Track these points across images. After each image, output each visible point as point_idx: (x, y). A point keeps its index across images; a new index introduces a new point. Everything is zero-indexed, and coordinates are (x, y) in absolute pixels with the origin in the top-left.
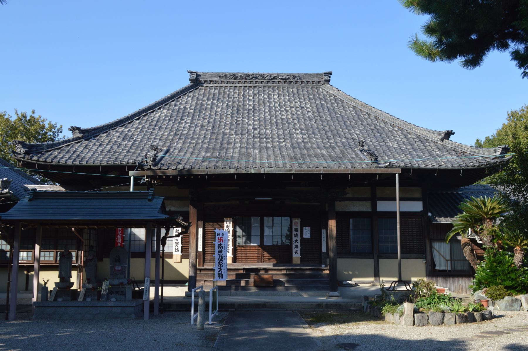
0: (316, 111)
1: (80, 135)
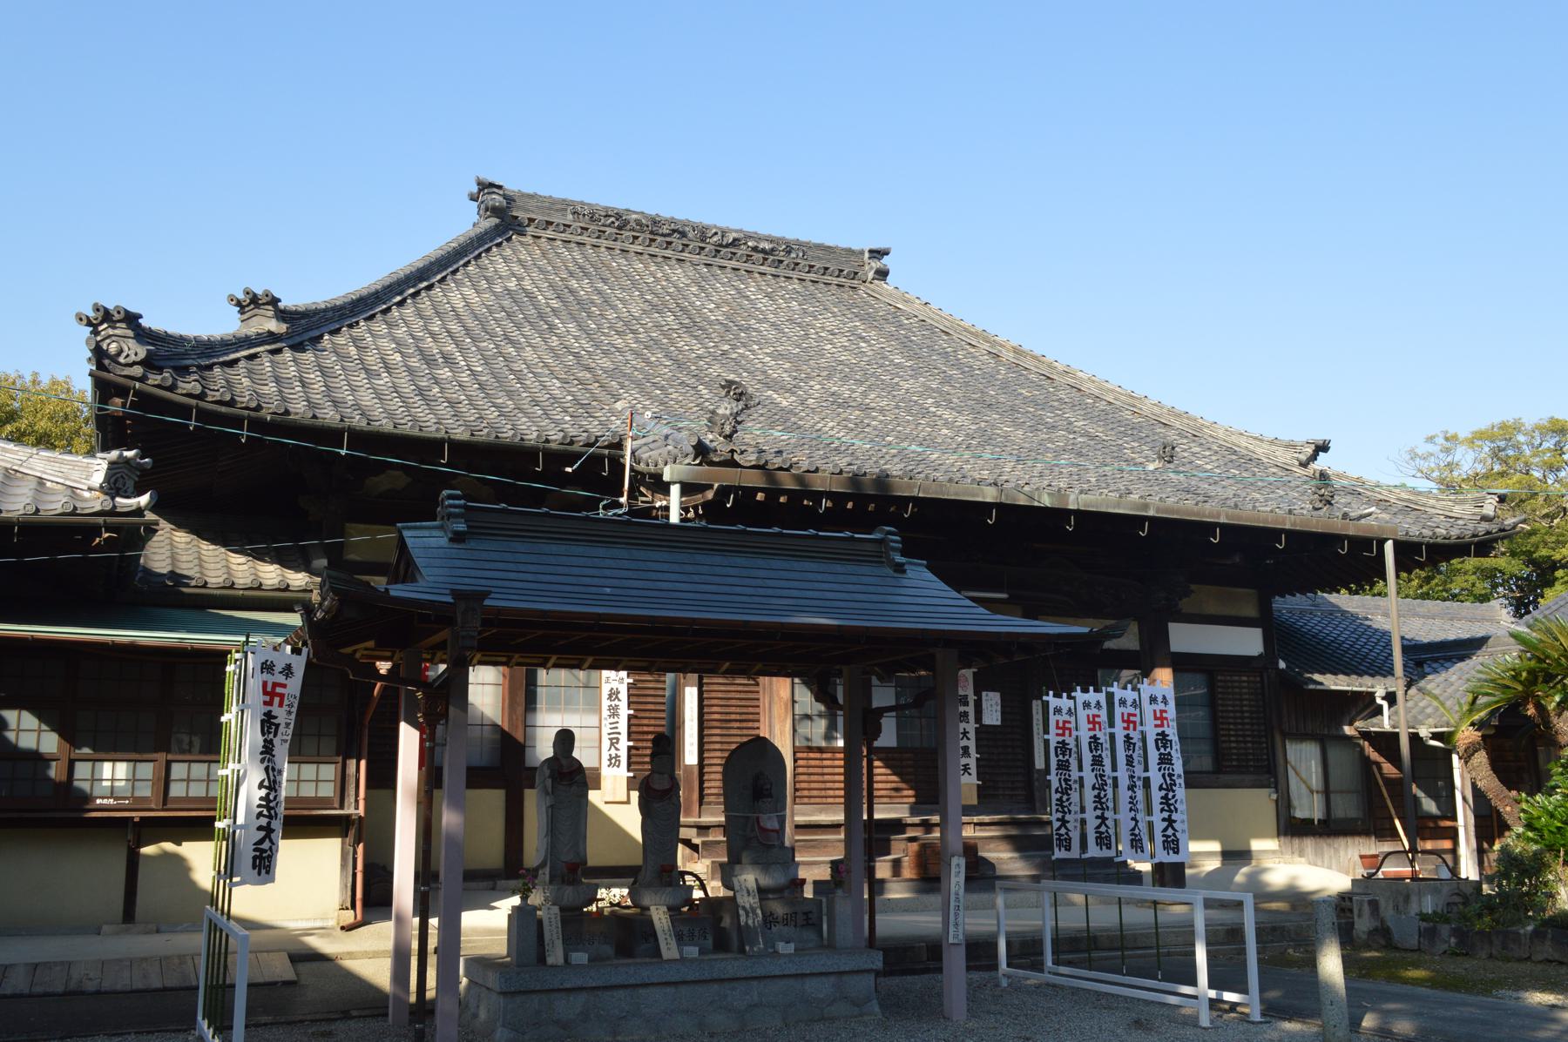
1: (274, 326)
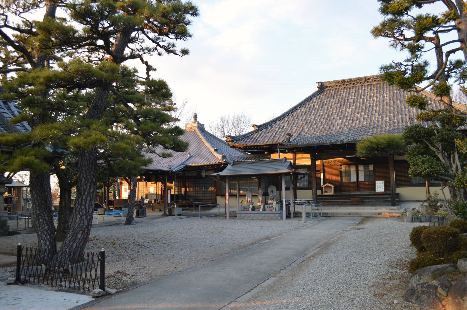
0: (392, 98)
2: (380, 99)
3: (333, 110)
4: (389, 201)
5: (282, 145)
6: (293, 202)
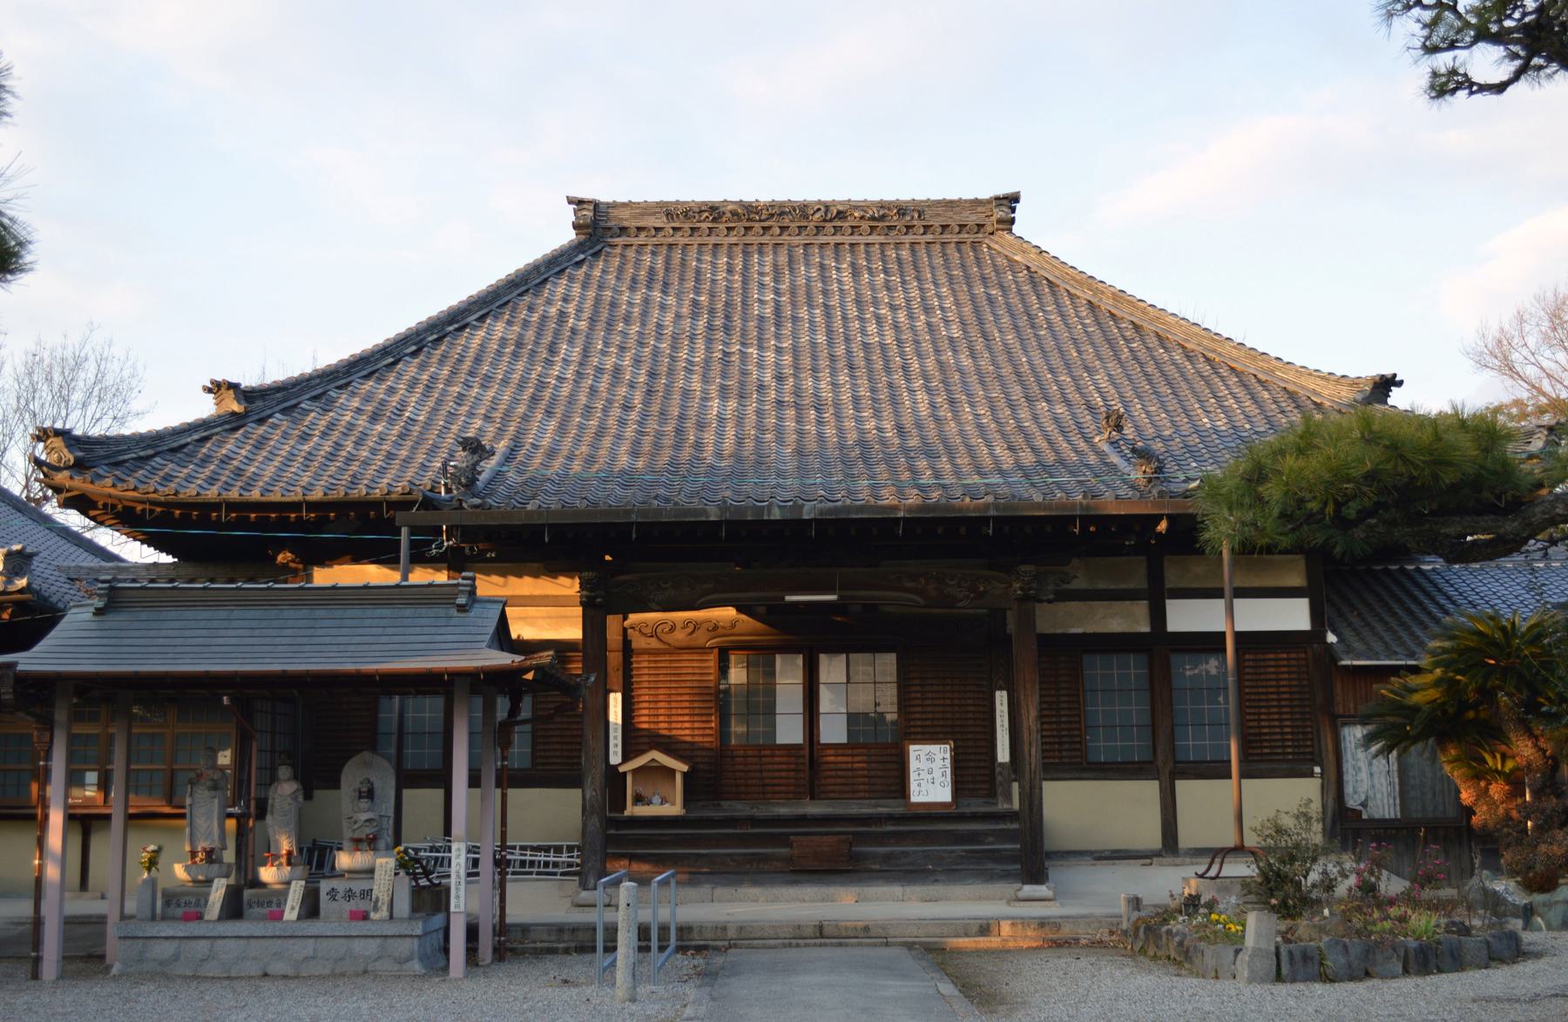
0: (971, 318)
2: (911, 317)
3: (674, 347)
4: (1013, 858)
5: (429, 503)
6: (497, 863)
